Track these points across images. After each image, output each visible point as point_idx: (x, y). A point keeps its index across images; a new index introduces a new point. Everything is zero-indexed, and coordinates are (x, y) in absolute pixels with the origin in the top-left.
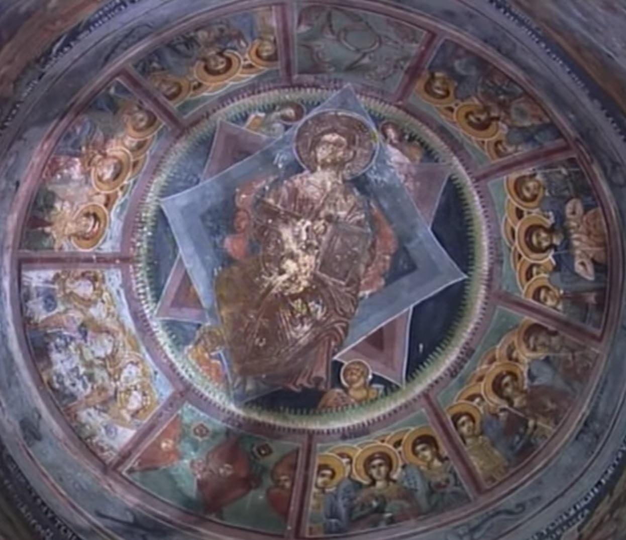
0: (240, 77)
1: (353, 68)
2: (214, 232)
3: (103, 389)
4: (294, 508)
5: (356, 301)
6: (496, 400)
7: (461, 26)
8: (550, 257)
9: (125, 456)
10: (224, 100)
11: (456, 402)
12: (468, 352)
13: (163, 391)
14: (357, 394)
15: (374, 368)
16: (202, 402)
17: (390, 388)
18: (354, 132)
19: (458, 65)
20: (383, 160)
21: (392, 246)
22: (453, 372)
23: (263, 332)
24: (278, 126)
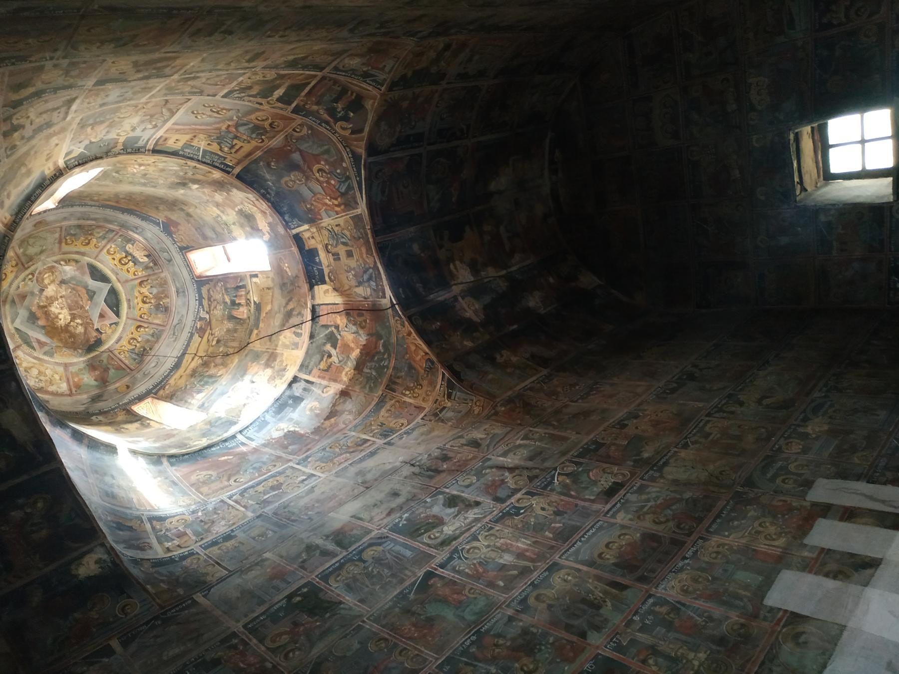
0: (11, 276)
1: (42, 252)
2: (34, 323)
3: (46, 381)
4: (123, 366)
5: (87, 311)
6: (147, 305)
7: (69, 220)
8: (131, 263)
9: (70, 390)
10: (10, 286)
11: (137, 313)
12: (129, 301)
13: (61, 369)
14: (109, 331)
15: (107, 322)
16: (72, 364)
17: (116, 324)
18: (51, 269)
19: (72, 232)
20: (64, 272)
21: (84, 291)
22: (129, 307)
23: (70, 337)
24: (29, 283)
